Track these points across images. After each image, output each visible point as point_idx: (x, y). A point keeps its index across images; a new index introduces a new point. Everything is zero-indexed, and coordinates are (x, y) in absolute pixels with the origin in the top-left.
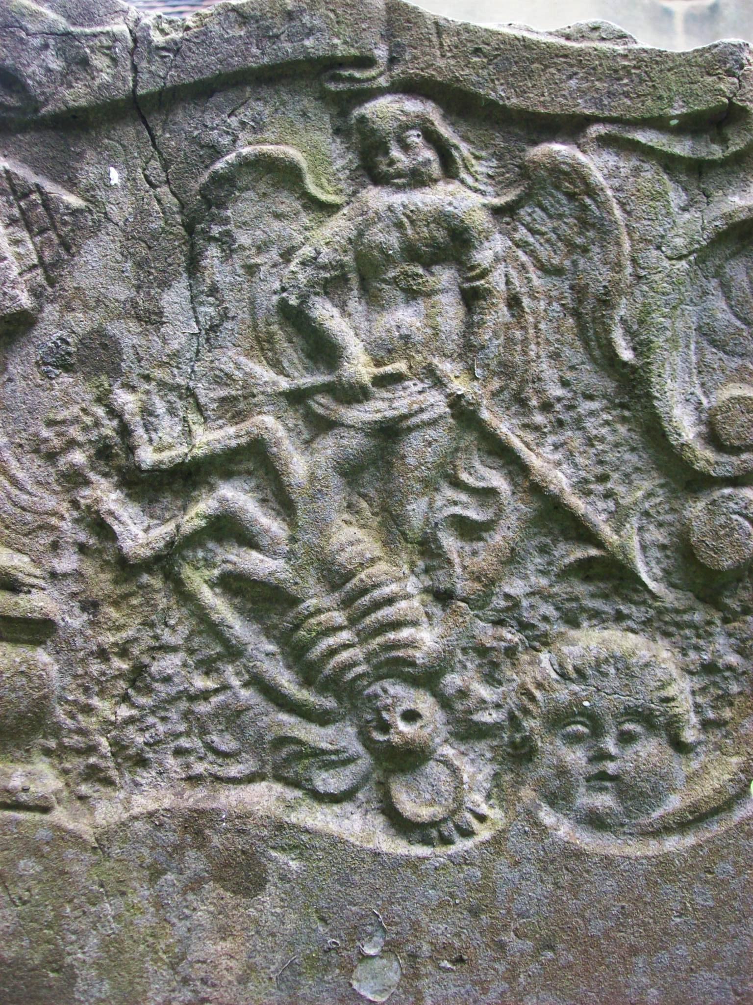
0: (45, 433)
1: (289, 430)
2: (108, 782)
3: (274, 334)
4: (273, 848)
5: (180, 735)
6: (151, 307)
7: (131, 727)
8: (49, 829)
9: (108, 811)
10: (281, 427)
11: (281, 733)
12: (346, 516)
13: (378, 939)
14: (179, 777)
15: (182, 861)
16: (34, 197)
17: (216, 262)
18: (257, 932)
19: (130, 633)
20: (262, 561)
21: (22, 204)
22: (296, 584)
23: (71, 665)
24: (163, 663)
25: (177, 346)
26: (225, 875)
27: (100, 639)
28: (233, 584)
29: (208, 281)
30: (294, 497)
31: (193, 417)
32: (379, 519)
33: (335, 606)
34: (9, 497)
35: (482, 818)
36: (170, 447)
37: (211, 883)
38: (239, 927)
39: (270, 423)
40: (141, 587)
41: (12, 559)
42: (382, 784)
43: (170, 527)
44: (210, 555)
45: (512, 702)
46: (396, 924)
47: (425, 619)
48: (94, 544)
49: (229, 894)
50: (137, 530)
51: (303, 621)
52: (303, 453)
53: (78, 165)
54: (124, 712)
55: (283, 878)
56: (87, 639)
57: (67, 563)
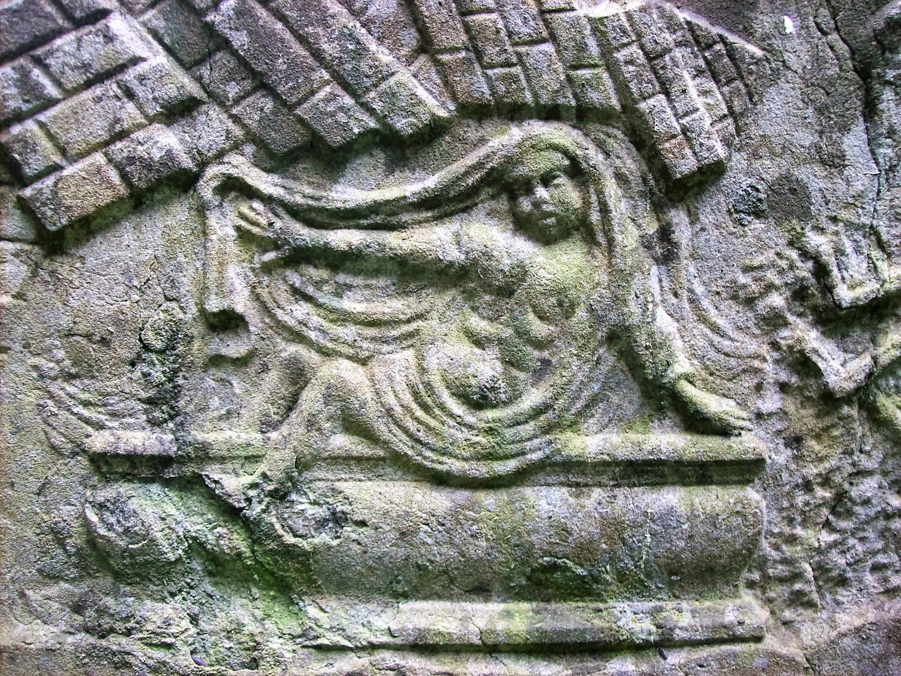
0: (742, 279)
2: (811, 605)
6: (834, 151)
7: (833, 551)
8: (765, 656)
9: (813, 631)
16: (718, 47)
17: (892, 105)
19: (833, 463)
21: (706, 54)
24: (862, 487)
25: (861, 188)
29: (886, 123)
31: (876, 254)
34: (712, 344)
36: (861, 284)
53: (752, 15)
54: (826, 537)
57: (771, 402)
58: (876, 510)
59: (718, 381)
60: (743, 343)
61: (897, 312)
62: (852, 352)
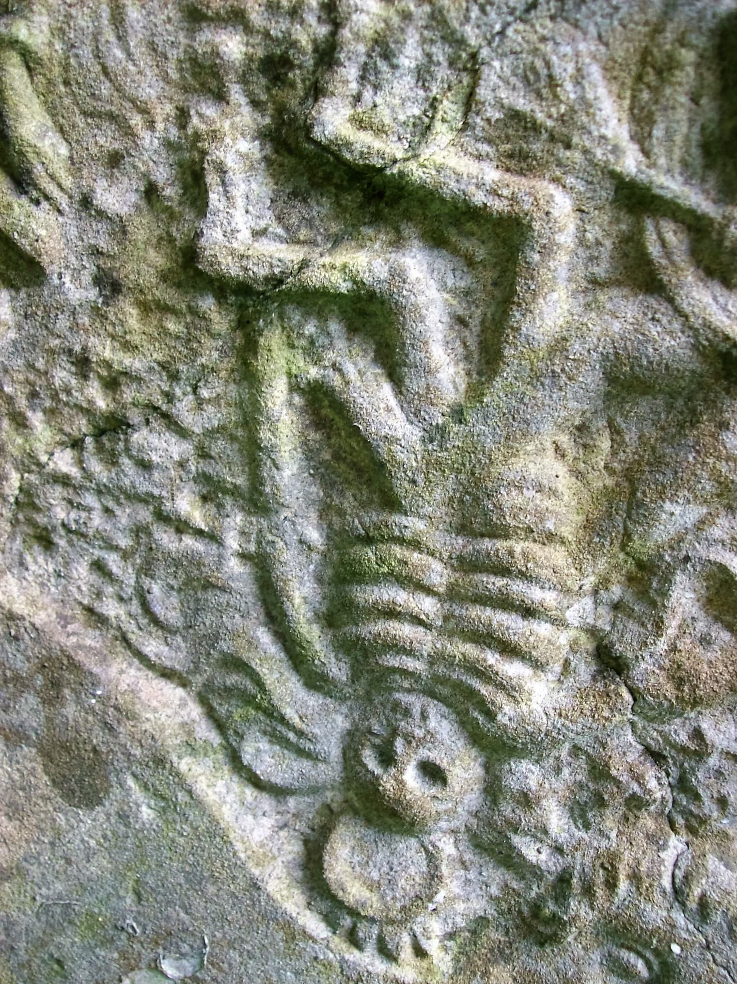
1: (582, 242)
3: (680, 66)
4: (134, 775)
5: (116, 548)
10: (571, 228)
11: (245, 656)
12: (564, 439)
13: (189, 965)
14: (79, 598)
15: (15, 697)
18: (52, 844)
19: (137, 365)
20: (389, 410)
22: (413, 482)
23: (34, 346)
24: (154, 440)
26: (55, 755)
27: (93, 341)
28: (324, 408)
30: (508, 352)
31: (450, 108)
32: (610, 482)
33: (446, 555)
35: (420, 952)
36: (380, 131)
37: (34, 750)
38: (34, 822)
39: (560, 211)
40: (193, 311)
41: (42, 137)
42: (331, 811)
43: (291, 255)
44: (322, 340)
45: (581, 861)
46: (220, 970)
47: (558, 668)
48: (170, 199)
49: (46, 778)
50: (242, 222)
51: (382, 540)
52: (574, 294)
54: (64, 462)
55: (123, 817)
56: (75, 327)
57: (116, 197)
58: (150, 489)
59: (67, 101)
60: (140, 73)
61: (403, 227)
62: (287, 229)
